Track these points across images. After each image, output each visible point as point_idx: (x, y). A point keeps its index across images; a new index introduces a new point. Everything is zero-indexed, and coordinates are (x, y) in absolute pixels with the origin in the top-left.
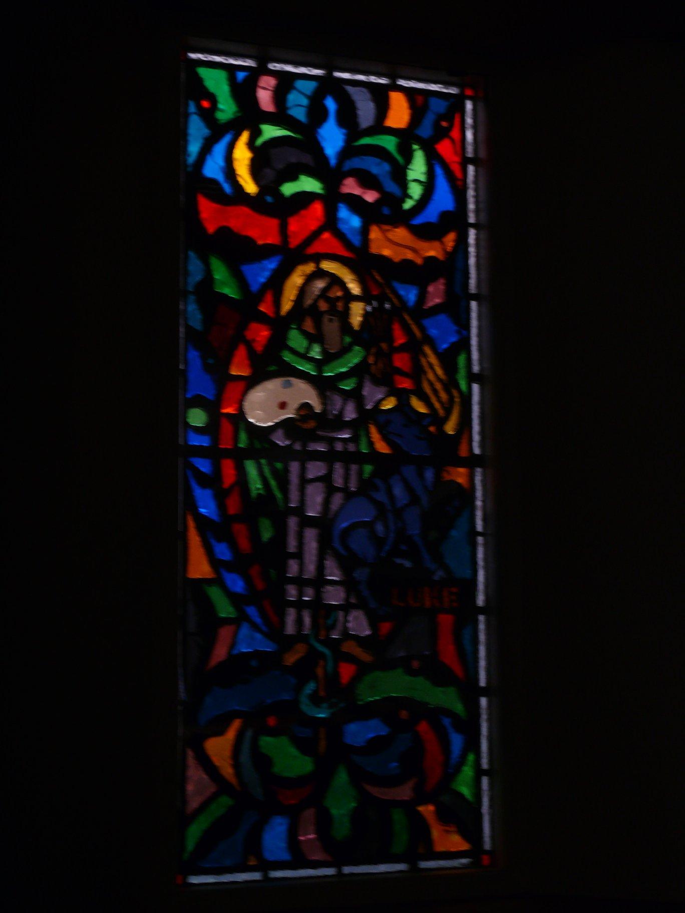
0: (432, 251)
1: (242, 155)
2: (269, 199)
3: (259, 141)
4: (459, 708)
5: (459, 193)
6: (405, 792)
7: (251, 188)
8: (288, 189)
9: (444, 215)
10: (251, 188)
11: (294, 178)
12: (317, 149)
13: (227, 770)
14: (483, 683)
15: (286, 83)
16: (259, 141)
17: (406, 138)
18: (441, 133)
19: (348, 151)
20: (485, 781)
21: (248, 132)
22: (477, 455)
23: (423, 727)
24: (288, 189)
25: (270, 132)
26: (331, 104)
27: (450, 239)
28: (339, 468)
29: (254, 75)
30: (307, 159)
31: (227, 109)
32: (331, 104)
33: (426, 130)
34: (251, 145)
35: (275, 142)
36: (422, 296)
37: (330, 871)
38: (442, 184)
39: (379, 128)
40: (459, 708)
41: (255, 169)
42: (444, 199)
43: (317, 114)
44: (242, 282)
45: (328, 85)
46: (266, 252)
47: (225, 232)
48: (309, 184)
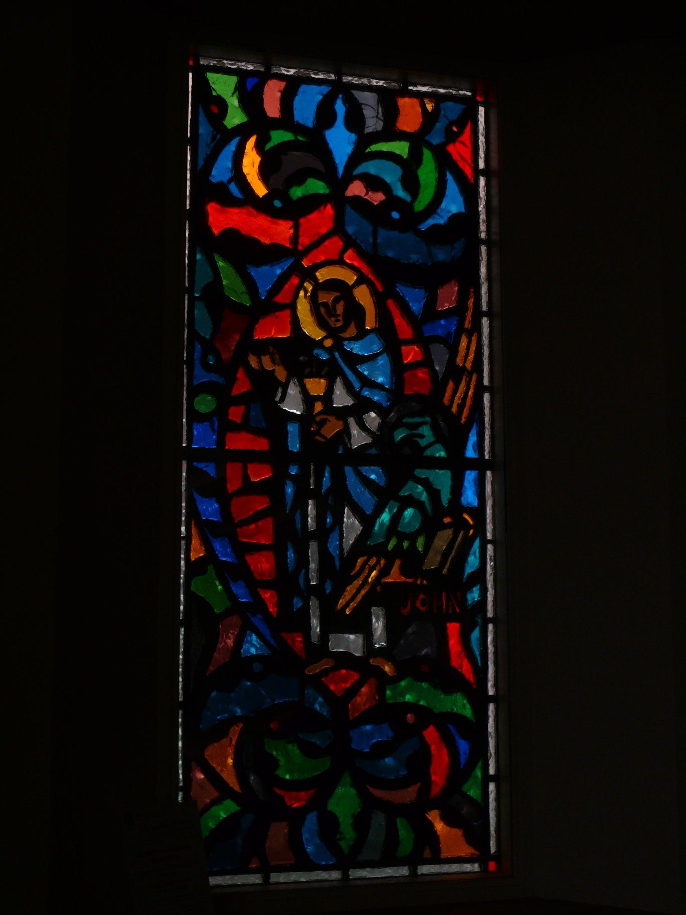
0: (441, 255)
1: (251, 162)
2: (278, 204)
3: (269, 146)
4: (468, 712)
5: (469, 193)
6: (410, 794)
7: (261, 190)
8: (297, 192)
9: (455, 218)
10: (261, 190)
11: (301, 182)
12: (326, 154)
13: (428, 453)
14: (491, 692)
15: (292, 87)
16: (269, 146)
17: (417, 140)
18: (451, 137)
19: (358, 156)
20: (492, 787)
21: (488, 538)
22: (350, 416)
23: (431, 734)
24: (297, 192)
25: (279, 137)
26: (340, 108)
27: (459, 245)
28: (261, 503)
29: (265, 77)
30: (318, 165)
31: (235, 117)
32: (340, 108)
33: (436, 139)
34: (259, 147)
35: (283, 147)
36: (431, 302)
37: (335, 875)
38: (452, 187)
39: (390, 133)
40: (468, 712)
41: (264, 173)
42: (453, 204)
43: (325, 116)
44: (251, 286)
45: (338, 89)
46: (274, 253)
47: (231, 234)
48: (316, 186)
